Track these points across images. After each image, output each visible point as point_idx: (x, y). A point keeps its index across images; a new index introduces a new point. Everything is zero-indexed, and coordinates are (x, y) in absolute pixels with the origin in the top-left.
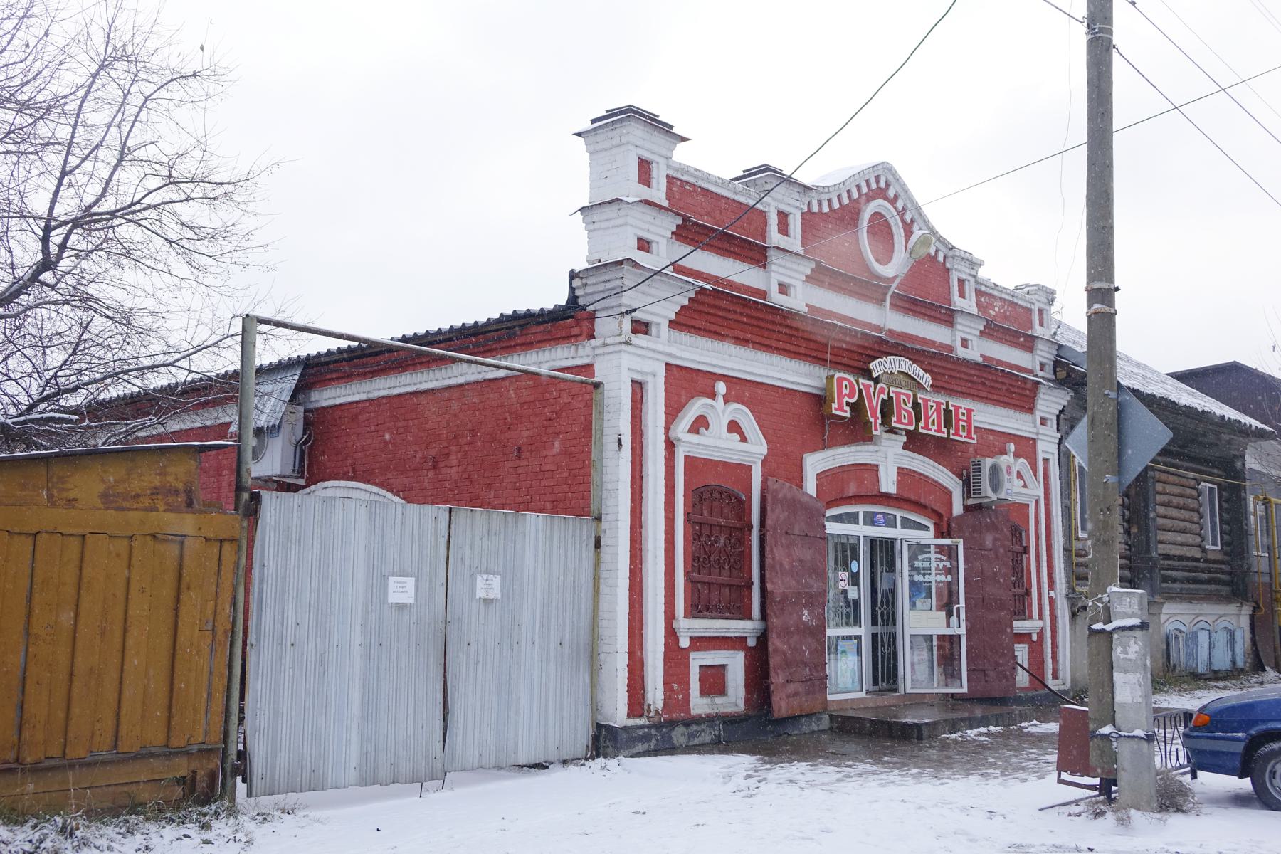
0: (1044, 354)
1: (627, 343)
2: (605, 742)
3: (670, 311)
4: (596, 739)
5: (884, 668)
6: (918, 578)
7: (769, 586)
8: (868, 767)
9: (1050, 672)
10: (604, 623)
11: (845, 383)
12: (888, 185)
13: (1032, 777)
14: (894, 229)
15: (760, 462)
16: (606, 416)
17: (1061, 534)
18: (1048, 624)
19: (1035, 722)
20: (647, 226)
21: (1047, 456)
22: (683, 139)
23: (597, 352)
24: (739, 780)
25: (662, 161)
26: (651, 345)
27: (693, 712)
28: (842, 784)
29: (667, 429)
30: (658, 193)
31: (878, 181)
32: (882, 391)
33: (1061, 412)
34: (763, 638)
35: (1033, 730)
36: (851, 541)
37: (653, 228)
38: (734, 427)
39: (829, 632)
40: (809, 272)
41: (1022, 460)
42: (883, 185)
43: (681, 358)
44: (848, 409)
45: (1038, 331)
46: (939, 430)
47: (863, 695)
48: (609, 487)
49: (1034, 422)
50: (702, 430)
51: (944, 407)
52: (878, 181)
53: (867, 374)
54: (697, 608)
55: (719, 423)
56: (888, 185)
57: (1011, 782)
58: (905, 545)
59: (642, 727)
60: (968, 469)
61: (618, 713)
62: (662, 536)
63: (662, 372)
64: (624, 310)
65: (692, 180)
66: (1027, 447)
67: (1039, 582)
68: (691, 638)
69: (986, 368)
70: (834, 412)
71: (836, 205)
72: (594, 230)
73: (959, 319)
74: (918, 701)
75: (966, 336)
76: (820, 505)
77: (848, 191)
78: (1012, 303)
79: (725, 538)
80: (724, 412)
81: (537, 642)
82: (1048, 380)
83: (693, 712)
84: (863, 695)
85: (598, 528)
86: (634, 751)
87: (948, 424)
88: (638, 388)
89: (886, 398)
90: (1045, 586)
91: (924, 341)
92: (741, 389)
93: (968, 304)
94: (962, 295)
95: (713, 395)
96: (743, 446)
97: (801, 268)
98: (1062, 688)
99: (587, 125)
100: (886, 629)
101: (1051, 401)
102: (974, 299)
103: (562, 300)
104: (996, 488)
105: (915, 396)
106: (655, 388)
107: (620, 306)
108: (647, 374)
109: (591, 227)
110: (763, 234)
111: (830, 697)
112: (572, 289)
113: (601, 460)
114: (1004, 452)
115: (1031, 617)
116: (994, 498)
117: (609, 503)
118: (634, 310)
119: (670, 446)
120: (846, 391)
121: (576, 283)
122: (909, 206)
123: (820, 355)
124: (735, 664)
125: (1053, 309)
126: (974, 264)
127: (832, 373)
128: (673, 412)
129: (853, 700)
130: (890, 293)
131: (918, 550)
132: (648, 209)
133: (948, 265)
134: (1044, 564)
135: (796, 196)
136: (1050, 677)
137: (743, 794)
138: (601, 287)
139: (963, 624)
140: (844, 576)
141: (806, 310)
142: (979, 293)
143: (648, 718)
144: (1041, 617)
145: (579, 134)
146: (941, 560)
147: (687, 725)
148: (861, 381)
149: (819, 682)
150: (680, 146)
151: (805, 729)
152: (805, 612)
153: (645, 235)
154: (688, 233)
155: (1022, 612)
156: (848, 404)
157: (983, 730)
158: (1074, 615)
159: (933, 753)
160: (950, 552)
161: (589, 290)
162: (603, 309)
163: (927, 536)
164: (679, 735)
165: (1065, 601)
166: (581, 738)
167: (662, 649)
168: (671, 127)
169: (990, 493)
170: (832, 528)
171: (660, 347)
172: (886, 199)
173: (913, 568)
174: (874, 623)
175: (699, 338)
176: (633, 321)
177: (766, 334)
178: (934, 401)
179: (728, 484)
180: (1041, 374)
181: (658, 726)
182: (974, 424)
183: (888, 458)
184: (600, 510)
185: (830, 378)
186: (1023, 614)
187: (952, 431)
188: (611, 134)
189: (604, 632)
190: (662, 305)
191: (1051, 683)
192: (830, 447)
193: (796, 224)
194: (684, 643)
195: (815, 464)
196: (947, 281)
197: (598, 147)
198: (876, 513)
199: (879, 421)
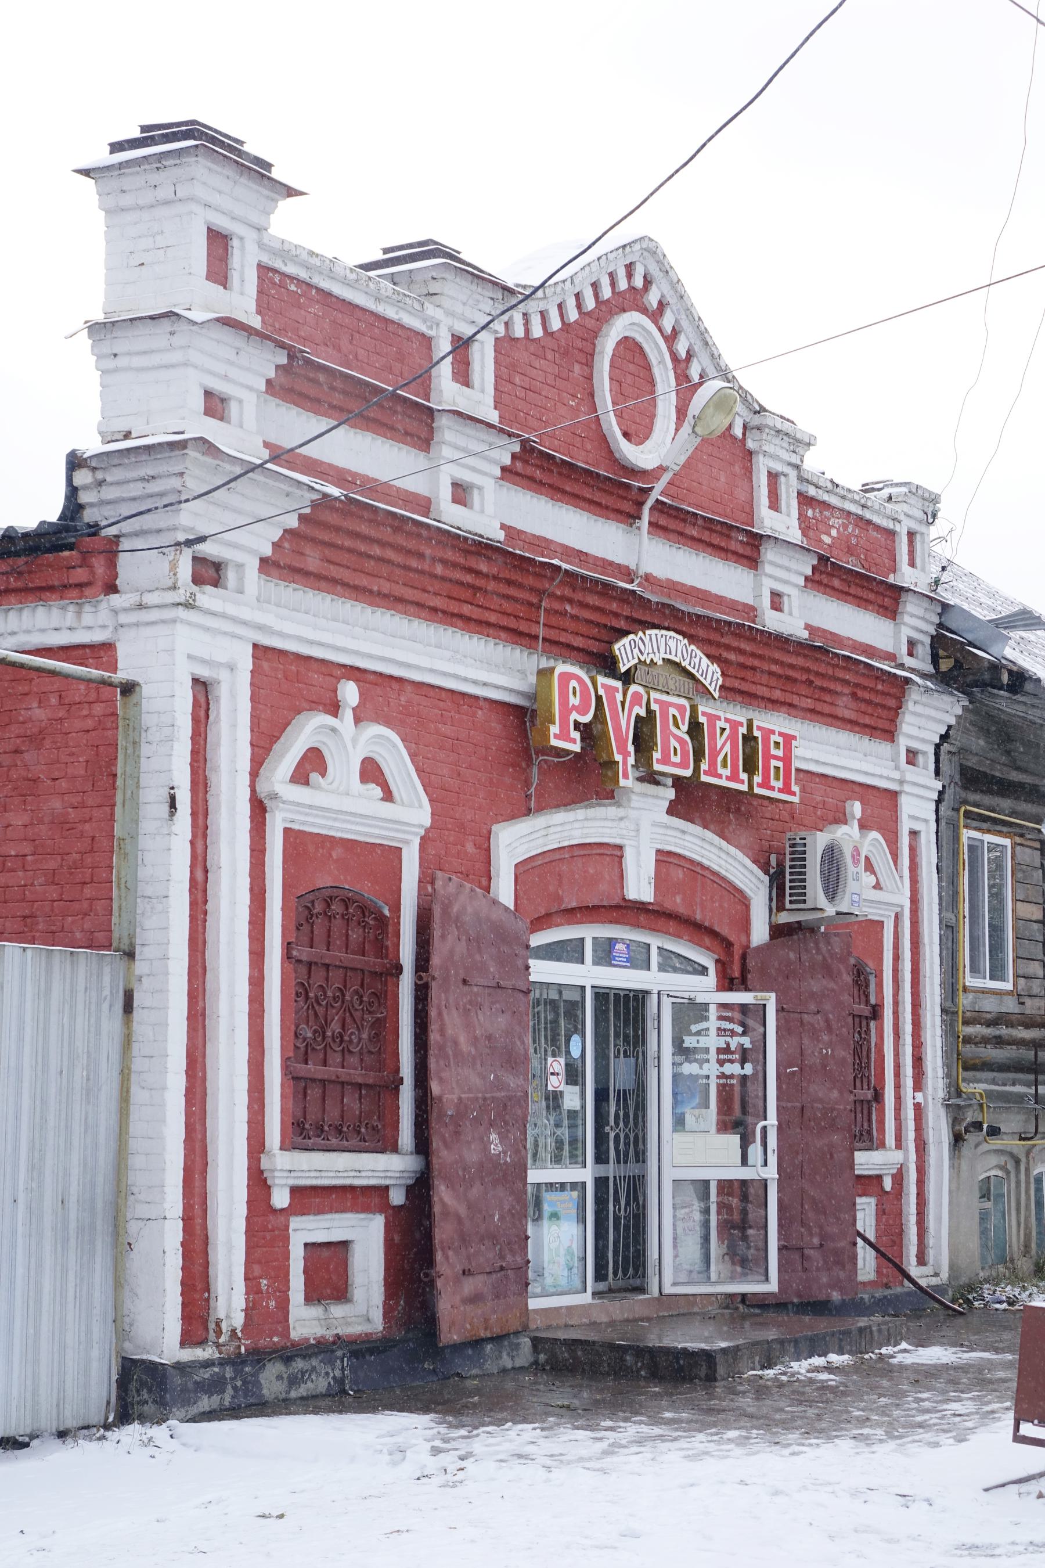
0: (916, 621)
1: (188, 605)
2: (141, 1392)
3: (263, 541)
4: (123, 1383)
5: (621, 1247)
6: (689, 1068)
7: (435, 1087)
8: (645, 1429)
9: (913, 1250)
10: (136, 1161)
11: (573, 683)
12: (648, 282)
13: (945, 1439)
14: (657, 371)
15: (417, 841)
16: (145, 750)
17: (937, 980)
18: (913, 1157)
19: (904, 1345)
20: (221, 368)
21: (917, 827)
22: (291, 192)
23: (123, 618)
24: (420, 1456)
25: (251, 235)
26: (231, 610)
27: (295, 1335)
28: (614, 1459)
29: (254, 774)
30: (242, 301)
31: (630, 276)
32: (637, 699)
33: (944, 738)
34: (420, 1188)
35: (908, 1359)
36: (567, 995)
37: (234, 373)
38: (371, 772)
39: (535, 1176)
40: (507, 461)
41: (875, 835)
42: (638, 282)
43: (281, 635)
44: (576, 735)
45: (906, 576)
46: (734, 777)
47: (586, 1298)
48: (149, 891)
49: (895, 759)
50: (314, 777)
51: (743, 730)
52: (630, 276)
53: (608, 664)
54: (303, 1133)
55: (344, 767)
56: (648, 282)
57: (913, 1448)
58: (667, 1004)
59: (207, 1364)
60: (781, 854)
61: (163, 1340)
62: (243, 989)
63: (246, 664)
64: (181, 537)
65: (303, 275)
66: (881, 808)
67: (897, 1074)
68: (295, 1191)
69: (818, 652)
70: (554, 742)
71: (556, 324)
72: (116, 370)
73: (769, 554)
74: (680, 1309)
75: (779, 587)
76: (521, 925)
77: (577, 296)
78: (860, 518)
79: (360, 992)
80: (355, 741)
81: (21, 1200)
82: (924, 676)
83: (295, 1335)
84: (586, 1298)
85: (129, 970)
86: (194, 1410)
87: (750, 767)
89: (643, 713)
90: (909, 1082)
92: (388, 696)
93: (780, 522)
94: (774, 504)
95: (334, 708)
96: (387, 810)
97: (495, 454)
98: (934, 1281)
99: (102, 157)
100: (623, 1170)
101: (929, 716)
102: (795, 513)
103: (51, 510)
104: (831, 894)
105: (694, 709)
106: (233, 696)
107: (175, 529)
108: (220, 665)
109: (111, 364)
110: (423, 381)
111: (533, 1304)
112: (72, 491)
113: (134, 837)
114: (840, 818)
115: (882, 1145)
116: (830, 910)
117: (148, 924)
118: (202, 539)
119: (259, 809)
120: (574, 701)
121: (82, 478)
122: (685, 324)
123: (523, 627)
124: (367, 1238)
125: (934, 531)
126: (799, 443)
127: (544, 663)
128: (264, 741)
129: (569, 1308)
130: (650, 503)
131: (690, 1012)
132: (227, 335)
133: (750, 444)
134: (908, 1040)
136: (913, 1260)
137: (436, 1481)
138: (136, 489)
139: (773, 1159)
140: (557, 1065)
141: (501, 535)
142: (805, 500)
143: (218, 1346)
144: (899, 1146)
145: (86, 172)
146: (733, 1034)
147: (287, 1360)
148: (601, 680)
149: (515, 1273)
150: (286, 205)
151: (490, 1366)
152: (494, 1137)
153: (219, 386)
154: (298, 384)
155: (868, 1137)
156: (577, 725)
157: (818, 1361)
158: (957, 1139)
159: (746, 1402)
160: (748, 1017)
161: (109, 493)
162: (136, 534)
163: (703, 987)
164: (271, 1380)
165: (942, 1112)
166: (98, 1388)
167: (242, 1210)
168: (268, 166)
169: (822, 901)
170: (544, 971)
171: (245, 613)
172: (644, 311)
173: (681, 1050)
174: (601, 1158)
175: (310, 593)
176: (195, 559)
178: (726, 716)
179: (367, 890)
180: (909, 662)
181: (236, 1361)
182: (796, 764)
183: (640, 830)
184: (132, 937)
185: (545, 674)
186: (869, 1139)
187: (758, 779)
188: (155, 178)
189: (137, 1179)
190: (248, 526)
191: (914, 1271)
192: (540, 809)
193: (484, 359)
194: (281, 1199)
195: (515, 842)
196: (748, 472)
197: (127, 200)
199: (631, 760)
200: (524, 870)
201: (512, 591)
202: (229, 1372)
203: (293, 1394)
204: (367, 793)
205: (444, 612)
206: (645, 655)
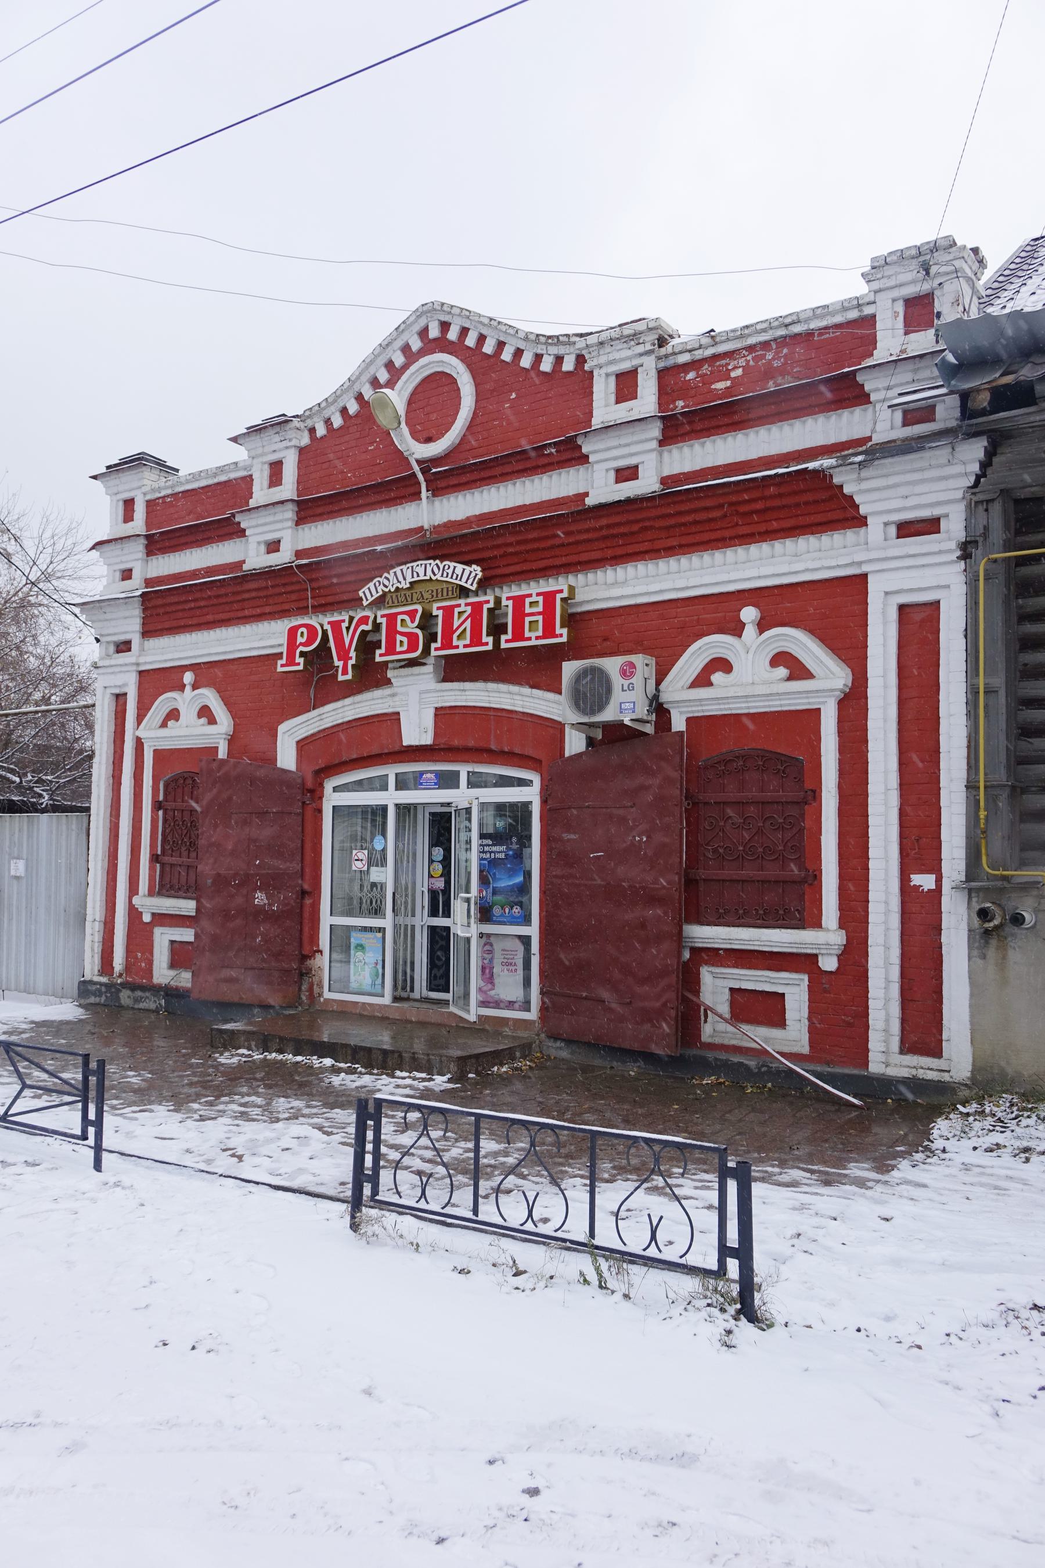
20: (118, 560)
37: (124, 559)
38: (205, 712)
65: (169, 492)
68: (153, 914)
88: (120, 698)
91: (345, 545)
92: (207, 673)
95: (181, 688)
115: (817, 924)
135: (277, 438)
177: (236, 606)
183: (416, 700)
198: (422, 773)
200: (302, 745)
201: (289, 588)
202: (103, 989)
203: (136, 1006)
204: (199, 723)
205: (665, 549)
206: (390, 587)
